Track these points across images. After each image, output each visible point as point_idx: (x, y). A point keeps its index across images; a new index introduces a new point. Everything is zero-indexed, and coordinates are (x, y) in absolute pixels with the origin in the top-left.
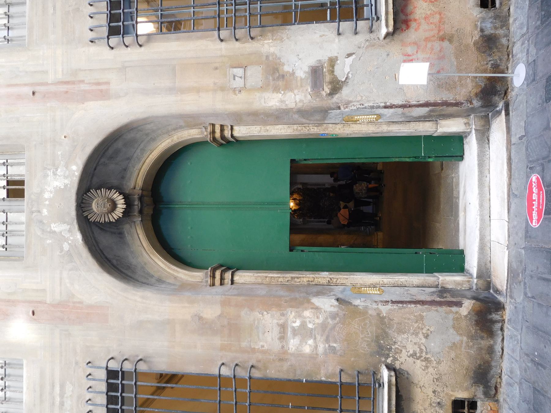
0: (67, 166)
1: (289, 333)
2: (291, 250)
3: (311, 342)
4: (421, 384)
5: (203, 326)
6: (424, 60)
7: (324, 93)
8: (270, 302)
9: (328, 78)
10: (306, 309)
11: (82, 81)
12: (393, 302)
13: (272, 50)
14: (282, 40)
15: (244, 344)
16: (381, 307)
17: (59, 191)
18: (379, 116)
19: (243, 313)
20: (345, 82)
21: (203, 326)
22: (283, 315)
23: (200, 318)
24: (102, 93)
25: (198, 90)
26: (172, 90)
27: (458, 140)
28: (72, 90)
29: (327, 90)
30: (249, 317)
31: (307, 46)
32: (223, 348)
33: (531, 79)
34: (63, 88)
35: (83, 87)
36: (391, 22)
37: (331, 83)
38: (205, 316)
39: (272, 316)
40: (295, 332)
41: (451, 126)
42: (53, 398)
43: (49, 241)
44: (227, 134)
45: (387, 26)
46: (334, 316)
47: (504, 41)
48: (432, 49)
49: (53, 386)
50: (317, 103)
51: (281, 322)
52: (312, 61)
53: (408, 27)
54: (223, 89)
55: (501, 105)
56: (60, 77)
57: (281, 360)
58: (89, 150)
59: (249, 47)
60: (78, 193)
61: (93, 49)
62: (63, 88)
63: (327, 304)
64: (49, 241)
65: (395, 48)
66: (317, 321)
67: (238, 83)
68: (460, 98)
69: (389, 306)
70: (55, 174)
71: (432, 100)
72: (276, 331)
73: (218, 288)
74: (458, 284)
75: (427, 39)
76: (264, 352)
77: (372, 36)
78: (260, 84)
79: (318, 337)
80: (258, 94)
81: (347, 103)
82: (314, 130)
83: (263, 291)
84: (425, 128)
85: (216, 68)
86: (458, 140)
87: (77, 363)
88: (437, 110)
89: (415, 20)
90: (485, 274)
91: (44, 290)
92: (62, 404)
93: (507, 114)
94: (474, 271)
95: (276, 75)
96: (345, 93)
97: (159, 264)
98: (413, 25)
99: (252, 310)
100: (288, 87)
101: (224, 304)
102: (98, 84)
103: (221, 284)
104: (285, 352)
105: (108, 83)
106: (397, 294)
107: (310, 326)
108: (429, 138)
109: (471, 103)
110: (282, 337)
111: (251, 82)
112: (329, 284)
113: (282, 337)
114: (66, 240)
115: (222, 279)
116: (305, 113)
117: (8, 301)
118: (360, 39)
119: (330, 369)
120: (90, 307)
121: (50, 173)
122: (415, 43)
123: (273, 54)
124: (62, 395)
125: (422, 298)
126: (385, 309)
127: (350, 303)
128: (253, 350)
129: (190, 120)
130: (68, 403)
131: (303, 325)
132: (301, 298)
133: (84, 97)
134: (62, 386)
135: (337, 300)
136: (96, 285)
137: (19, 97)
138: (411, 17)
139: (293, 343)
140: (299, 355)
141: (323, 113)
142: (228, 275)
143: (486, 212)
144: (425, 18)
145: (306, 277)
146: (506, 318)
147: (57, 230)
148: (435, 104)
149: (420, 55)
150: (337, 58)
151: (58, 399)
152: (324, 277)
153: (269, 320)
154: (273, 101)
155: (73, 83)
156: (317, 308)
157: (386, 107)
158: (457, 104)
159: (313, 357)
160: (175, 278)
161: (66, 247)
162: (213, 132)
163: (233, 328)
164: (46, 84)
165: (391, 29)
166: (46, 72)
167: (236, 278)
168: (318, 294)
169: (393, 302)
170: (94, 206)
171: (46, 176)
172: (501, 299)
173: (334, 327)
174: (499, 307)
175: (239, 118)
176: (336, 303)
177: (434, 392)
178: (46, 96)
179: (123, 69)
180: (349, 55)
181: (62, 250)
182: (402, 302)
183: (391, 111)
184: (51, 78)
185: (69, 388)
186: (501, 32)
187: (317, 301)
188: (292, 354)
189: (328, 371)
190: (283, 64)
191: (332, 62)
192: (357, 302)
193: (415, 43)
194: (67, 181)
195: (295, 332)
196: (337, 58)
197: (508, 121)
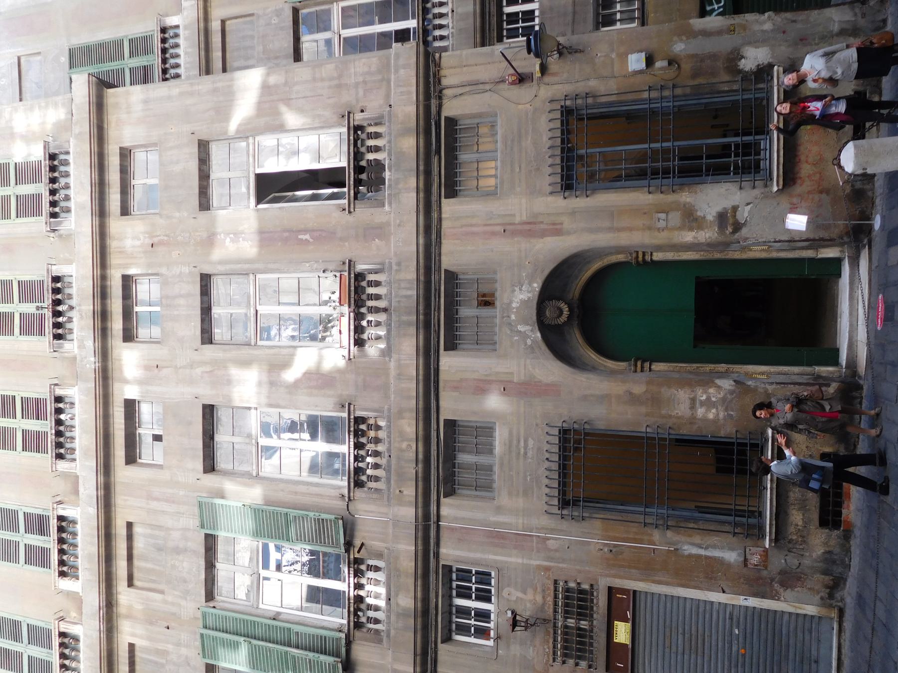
0: (530, 284)
1: (698, 405)
2: (695, 346)
3: (714, 411)
4: (797, 441)
5: (633, 399)
6: (804, 214)
7: (728, 232)
8: (683, 383)
9: (731, 221)
10: (711, 387)
11: (542, 222)
12: (777, 383)
13: (688, 200)
14: (696, 193)
15: (663, 412)
16: (767, 386)
17: (523, 302)
18: (770, 246)
19: (663, 390)
20: (744, 224)
21: (633, 399)
22: (693, 391)
23: (631, 393)
24: (557, 231)
25: (631, 229)
26: (611, 229)
27: (838, 262)
28: (531, 228)
29: (730, 229)
30: (666, 392)
31: (714, 198)
32: (647, 415)
33: (882, 226)
34: (527, 227)
35: (542, 226)
36: (781, 182)
37: (733, 224)
38: (634, 392)
39: (685, 392)
40: (702, 404)
41: (830, 253)
42: (519, 450)
43: (516, 338)
44: (648, 258)
45: (778, 185)
46: (731, 392)
47: (870, 194)
48: (813, 199)
49: (519, 441)
50: (721, 239)
51: (691, 396)
52: (719, 208)
53: (794, 183)
54: (650, 228)
55: (866, 241)
56: (524, 218)
57: (691, 423)
58: (547, 272)
59: (670, 198)
60: (538, 304)
61: (550, 199)
62: (527, 227)
63: (726, 384)
64: (516, 338)
65: (784, 201)
66: (719, 396)
67: (662, 224)
68: (834, 236)
69: (774, 386)
70: (521, 290)
71: (812, 237)
72: (688, 402)
73: (639, 374)
74: (831, 372)
75: (809, 192)
76: (679, 418)
77: (767, 190)
78: (679, 225)
79: (720, 408)
80: (676, 233)
81: (746, 239)
82: (718, 256)
83: (677, 376)
84: (809, 254)
85: (645, 213)
86: (838, 262)
87: (537, 425)
88: (814, 243)
89: (801, 178)
90: (852, 364)
91: (512, 373)
92: (526, 453)
93: (870, 248)
94: (844, 363)
95: (691, 219)
96: (744, 232)
97: (592, 356)
98: (799, 181)
99: (670, 387)
100: (700, 228)
101: (649, 383)
102: (554, 224)
103: (642, 371)
104: (695, 418)
105: (561, 224)
106: (781, 379)
107: (714, 399)
108: (811, 260)
109: (842, 239)
110: (693, 407)
111: (671, 224)
112: (727, 371)
113: (693, 407)
114: (529, 337)
115: (642, 367)
116: (711, 246)
117: (485, 381)
118: (756, 192)
119: (728, 430)
120: (547, 385)
121: (517, 289)
122: (799, 195)
123: (689, 203)
124: (526, 447)
125: (800, 381)
126: (770, 388)
127: (744, 384)
128: (670, 416)
129: (619, 250)
130: (530, 454)
131: (709, 398)
132: (707, 381)
133: (543, 234)
134: (526, 441)
135: (735, 381)
136: (551, 370)
137: (494, 234)
138: (798, 175)
139: (700, 412)
140: (705, 420)
141: (726, 245)
142: (647, 365)
143: (855, 319)
144: (808, 177)
145: (709, 367)
146: (864, 395)
147: (522, 330)
148: (814, 240)
149: (804, 204)
150: (738, 206)
151: (522, 451)
152: (722, 367)
153: (683, 395)
154: (689, 237)
155: (534, 223)
156: (719, 387)
157: (775, 242)
158: (831, 240)
159: (715, 421)
160: (605, 366)
161: (529, 342)
162: (637, 257)
163: (655, 401)
164: (514, 224)
165: (781, 187)
166: (514, 215)
167: (653, 367)
168: (719, 378)
169: (777, 383)
170: (548, 313)
171: (514, 291)
172: (861, 382)
173: (731, 401)
174: (860, 388)
175: (659, 248)
176: (733, 383)
177: (807, 447)
178: (514, 233)
179: (573, 213)
180: (748, 204)
181: (526, 344)
182: (784, 383)
183: (779, 244)
184: (517, 220)
185: (531, 443)
186: (867, 187)
187: (719, 382)
188: (699, 419)
189: (727, 431)
190: (697, 211)
191: (735, 209)
192: (750, 383)
193: (799, 195)
194: (530, 295)
195: (702, 404)
196: (738, 206)
197: (870, 254)
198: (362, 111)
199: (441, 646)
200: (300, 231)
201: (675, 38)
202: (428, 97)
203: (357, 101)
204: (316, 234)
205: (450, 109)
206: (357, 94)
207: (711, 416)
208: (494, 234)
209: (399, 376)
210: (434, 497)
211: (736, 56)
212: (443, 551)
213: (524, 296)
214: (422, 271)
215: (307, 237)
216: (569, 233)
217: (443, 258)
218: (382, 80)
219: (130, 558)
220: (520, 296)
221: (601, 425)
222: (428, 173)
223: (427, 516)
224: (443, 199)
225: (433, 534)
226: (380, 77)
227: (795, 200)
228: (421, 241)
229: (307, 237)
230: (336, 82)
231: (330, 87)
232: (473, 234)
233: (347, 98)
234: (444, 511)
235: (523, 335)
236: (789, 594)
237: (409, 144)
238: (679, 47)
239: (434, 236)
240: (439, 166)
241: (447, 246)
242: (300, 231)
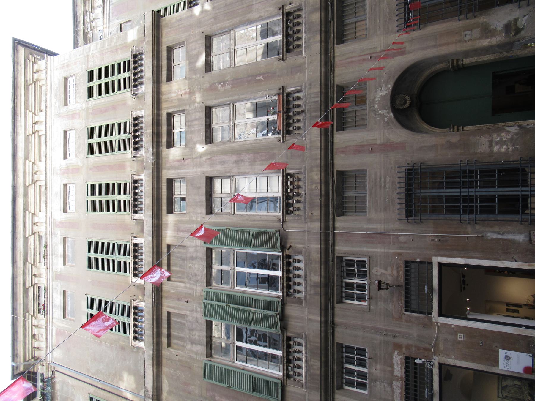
24: (402, 52)
25: (447, 44)
40: (497, 143)
56: (382, 48)
58: (396, 77)
92: (385, 186)
95: (487, 31)
134: (385, 178)
137: (364, 60)
139: (496, 148)
159: (506, 153)
184: (378, 143)
185: (388, 179)
207: (503, 150)
208: (364, 60)
209: (310, 149)
212: (337, 248)
213: (382, 93)
214: (323, 87)
215: (261, 78)
216: (409, 52)
217: (336, 79)
219: (169, 328)
220: (380, 93)
221: (431, 163)
222: (327, 32)
225: (331, 238)
228: (323, 70)
229: (261, 78)
232: (352, 62)
235: (383, 116)
237: (316, 17)
239: (330, 67)
240: (333, 28)
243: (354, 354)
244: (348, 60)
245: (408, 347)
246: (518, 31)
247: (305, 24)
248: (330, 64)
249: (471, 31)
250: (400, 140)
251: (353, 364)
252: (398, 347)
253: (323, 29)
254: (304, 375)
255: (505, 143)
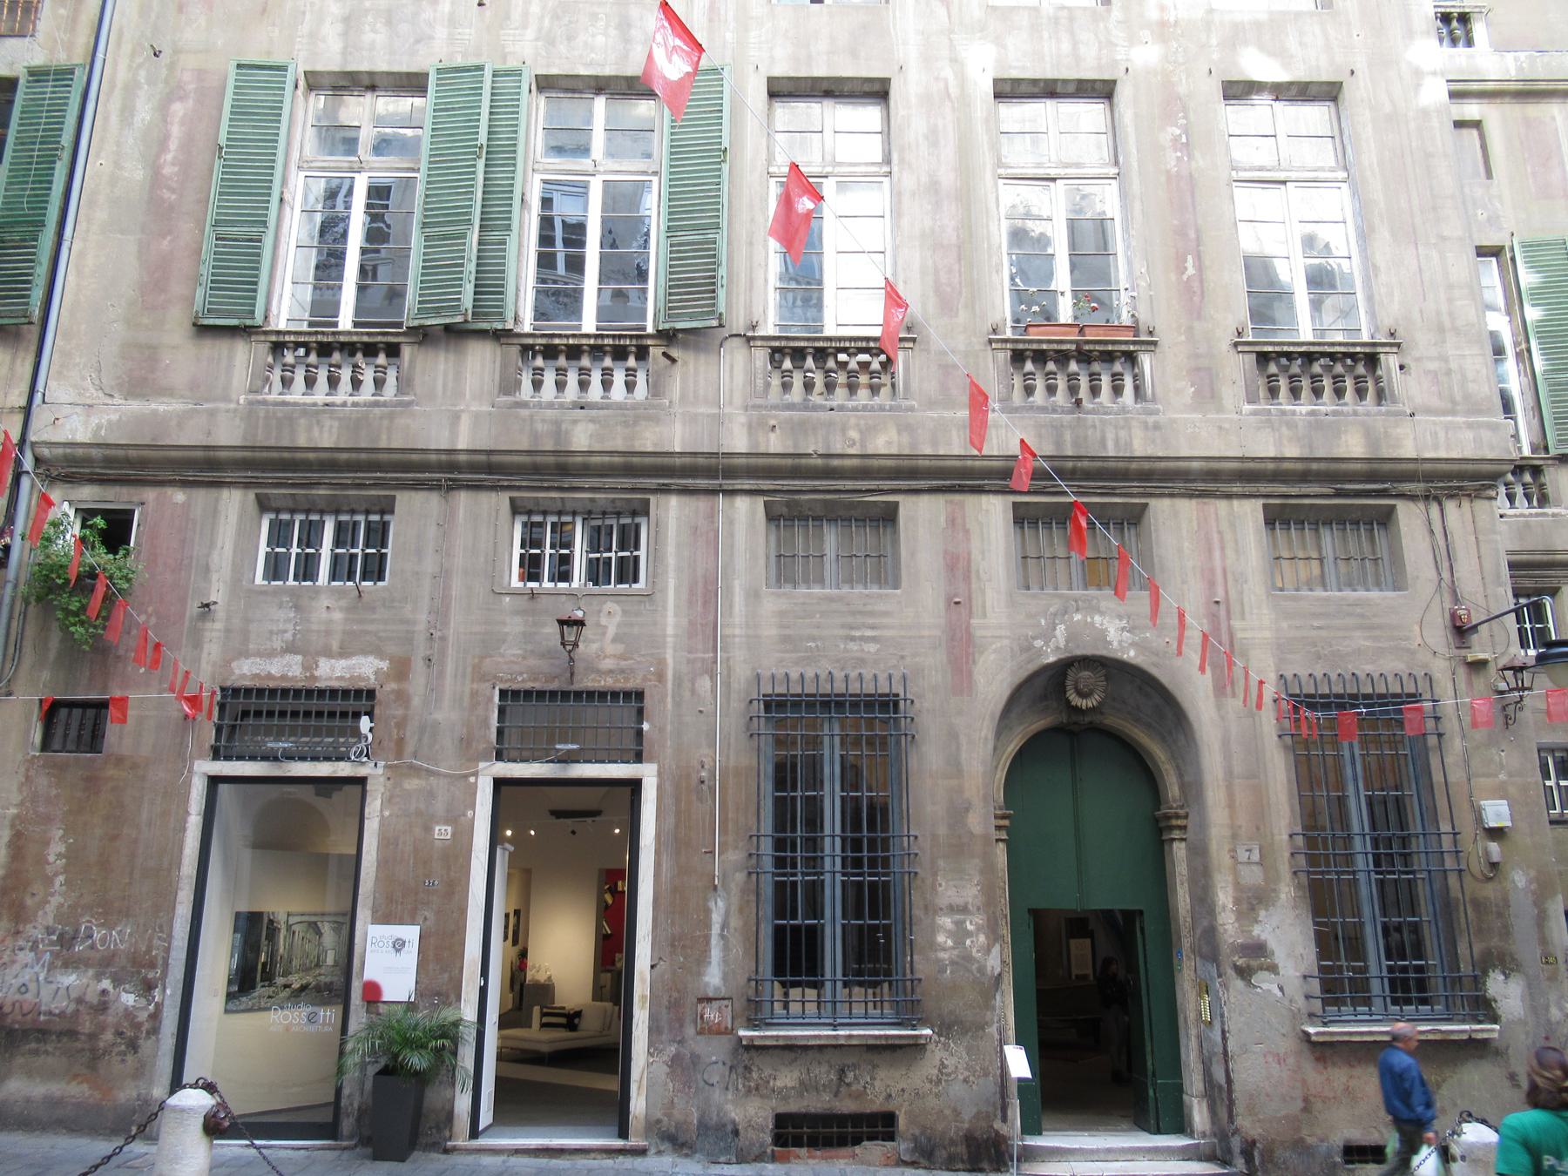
25: (1231, 805)
56: (1239, 635)
67: (1243, 856)
92: (853, 639)
95: (1253, 902)
130: (853, 646)
134: (873, 639)
136: (995, 678)
137: (1212, 584)
139: (946, 921)
159: (933, 946)
184: (1236, 624)
185: (872, 648)
198: (1402, 368)
199: (503, 499)
200: (1199, 258)
201: (1533, 873)
202: (1429, 477)
203: (1418, 360)
204: (1196, 285)
205: (1409, 517)
206: (1431, 359)
207: (941, 938)
208: (1212, 584)
210: (766, 484)
211: (1508, 965)
215: (1191, 271)
216: (1219, 707)
217: (1166, 502)
218: (1454, 402)
220: (1114, 629)
222: (1304, 477)
223: (730, 473)
224: (1261, 502)
225: (702, 483)
226: (1458, 398)
227: (1291, 1061)
228: (1195, 465)
229: (1191, 271)
230: (1447, 324)
231: (1438, 313)
232: (1210, 551)
233: (1421, 343)
234: (742, 503)
235: (1048, 635)
236: (662, 1070)
237: (1352, 446)
238: (1519, 879)
240: (1315, 495)
241: (1187, 507)
242: (1199, 258)
243: (367, 545)
244: (1216, 536)
245: (402, 697)
246: (1244, 973)
247: (1335, 413)
248: (1211, 486)
249: (1260, 864)
250: (980, 679)
251: (338, 542)
252: (401, 669)
253: (1315, 466)
254: (288, 398)
255: (959, 943)
